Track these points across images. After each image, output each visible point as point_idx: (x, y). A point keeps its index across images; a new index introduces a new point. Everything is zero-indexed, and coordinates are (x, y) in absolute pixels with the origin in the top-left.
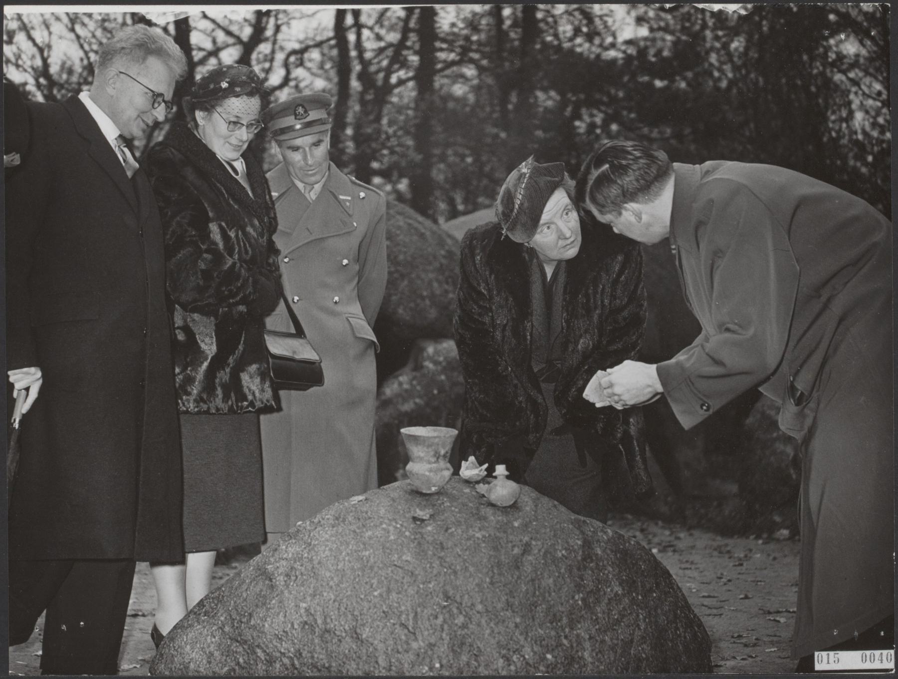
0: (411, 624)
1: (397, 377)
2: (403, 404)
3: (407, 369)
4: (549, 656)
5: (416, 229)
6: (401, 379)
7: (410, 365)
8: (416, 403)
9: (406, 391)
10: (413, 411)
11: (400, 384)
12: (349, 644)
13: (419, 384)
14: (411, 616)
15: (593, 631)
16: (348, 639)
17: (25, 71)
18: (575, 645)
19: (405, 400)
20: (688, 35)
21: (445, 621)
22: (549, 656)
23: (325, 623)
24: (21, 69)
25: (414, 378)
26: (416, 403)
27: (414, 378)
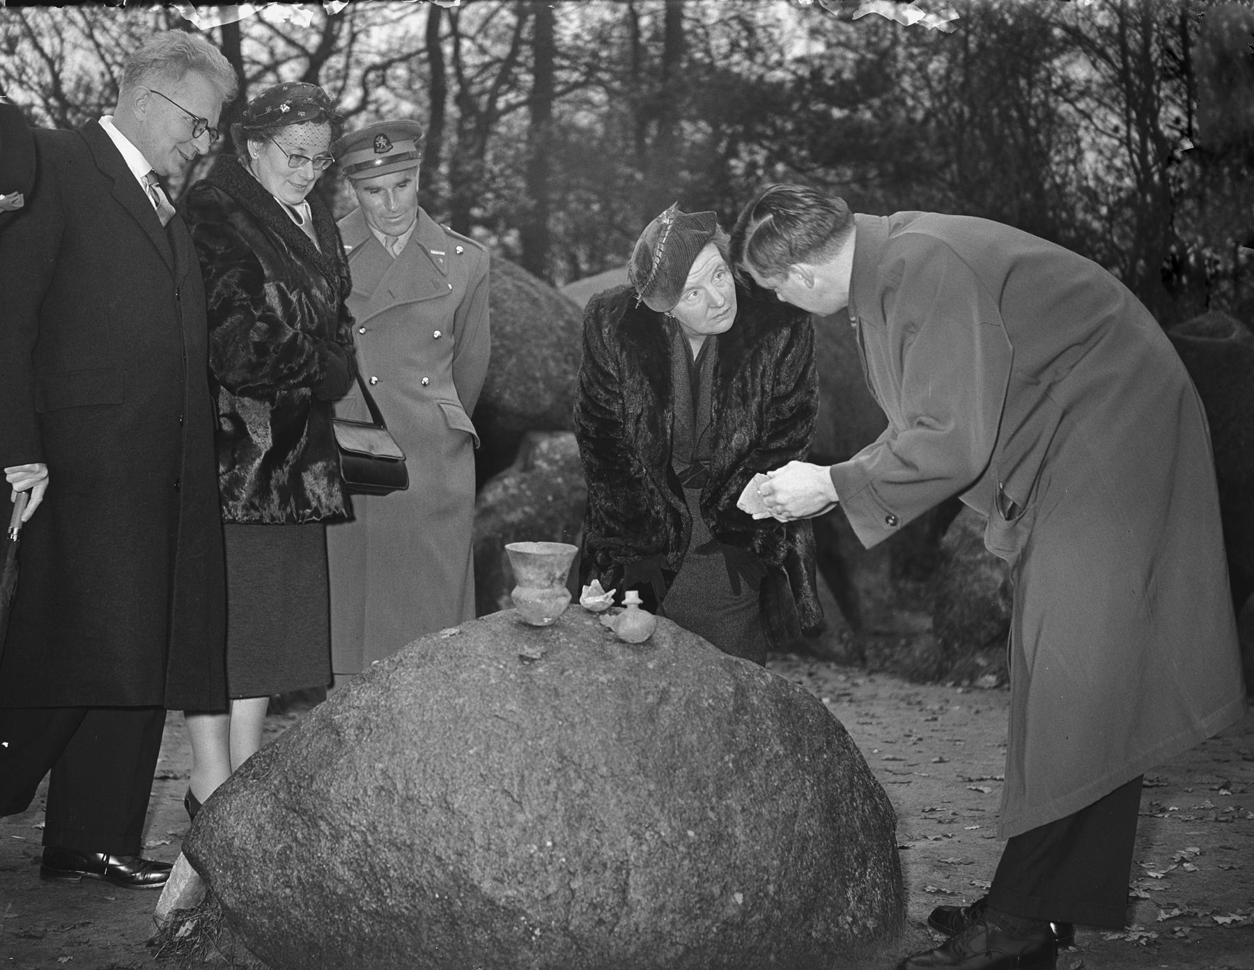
2: (508, 513)
4: (691, 833)
5: (527, 294)
6: (506, 481)
7: (519, 464)
8: (525, 513)
9: (513, 496)
10: (521, 522)
11: (506, 488)
12: (436, 816)
13: (529, 488)
14: (516, 780)
15: (747, 801)
23: (406, 788)
25: (523, 481)
27: (523, 481)
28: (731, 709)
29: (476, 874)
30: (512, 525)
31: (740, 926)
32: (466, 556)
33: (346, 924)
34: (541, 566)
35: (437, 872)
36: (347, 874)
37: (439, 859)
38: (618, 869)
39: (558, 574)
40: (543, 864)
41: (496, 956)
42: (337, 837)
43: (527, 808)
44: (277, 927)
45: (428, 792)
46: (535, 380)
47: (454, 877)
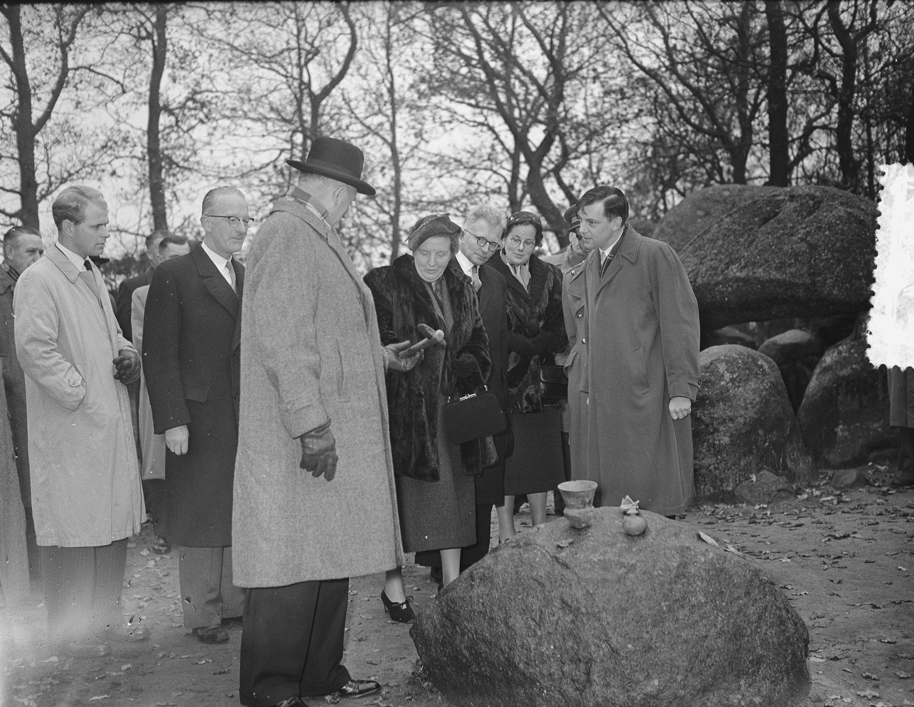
0: (538, 619)
1: (838, 346)
2: (841, 370)
3: (848, 340)
4: (630, 646)
5: (856, 217)
6: (840, 348)
7: (852, 336)
8: (852, 368)
9: (845, 358)
10: (850, 375)
11: (840, 353)
12: (502, 627)
13: (856, 352)
14: (538, 613)
15: (673, 628)
16: (502, 625)
17: (111, 231)
18: (654, 638)
19: (843, 366)
20: (832, 106)
21: (559, 618)
22: (630, 646)
23: (491, 613)
24: (115, 229)
25: (853, 347)
26: (852, 368)
27: (853, 347)
28: (672, 576)
29: (517, 660)
30: (844, 378)
31: (655, 697)
32: (393, 544)
33: (467, 677)
34: (578, 498)
35: (501, 657)
36: (466, 653)
37: (501, 650)
38: (587, 663)
39: (587, 501)
40: (548, 657)
41: (527, 701)
42: (463, 634)
43: (542, 629)
44: (442, 675)
45: (499, 615)
46: (859, 278)
47: (508, 660)
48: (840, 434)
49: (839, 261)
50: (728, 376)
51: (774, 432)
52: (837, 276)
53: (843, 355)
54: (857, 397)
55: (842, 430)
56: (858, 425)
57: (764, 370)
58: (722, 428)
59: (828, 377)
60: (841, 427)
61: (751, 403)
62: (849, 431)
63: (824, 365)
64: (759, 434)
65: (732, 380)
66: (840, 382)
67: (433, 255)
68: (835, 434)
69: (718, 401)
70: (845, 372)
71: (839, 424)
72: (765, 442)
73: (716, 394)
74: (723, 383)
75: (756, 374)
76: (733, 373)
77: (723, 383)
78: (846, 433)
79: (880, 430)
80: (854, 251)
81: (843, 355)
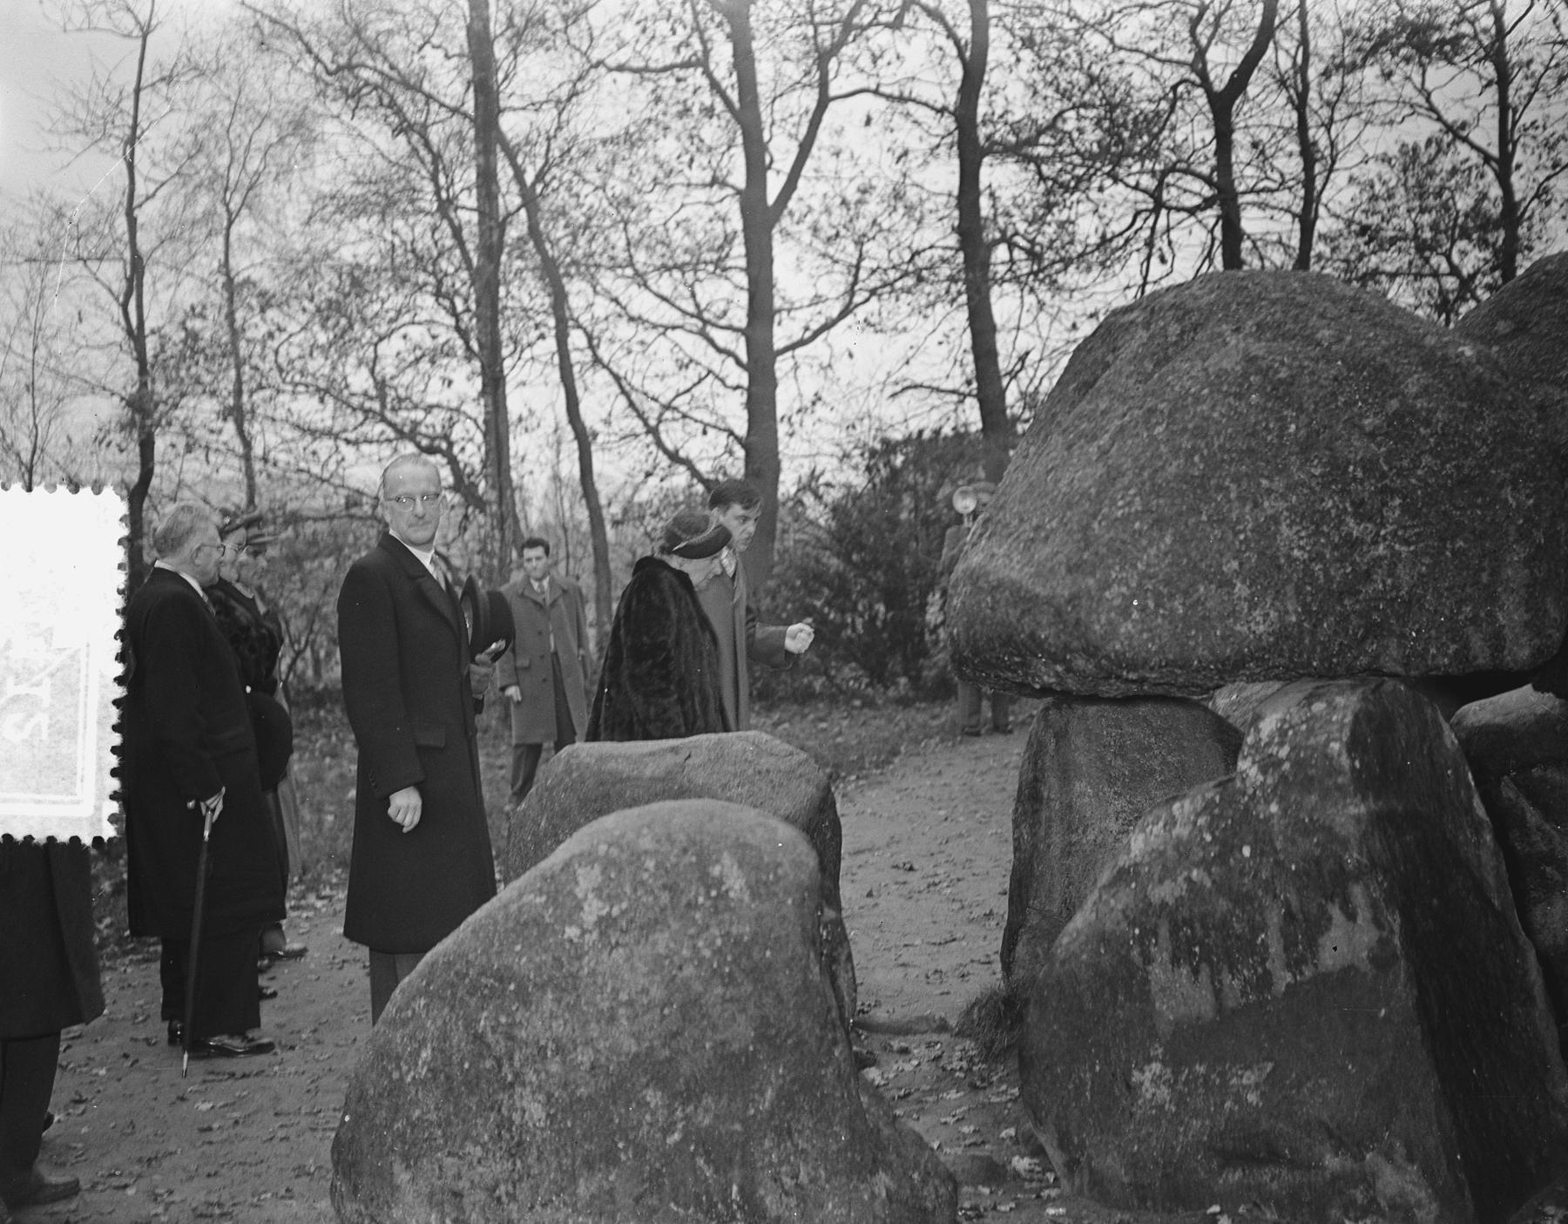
11: (1171, 822)
19: (1167, 873)
26: (1189, 880)
48: (1148, 1090)
49: (1159, 523)
50: (593, 910)
51: (708, 1100)
52: (1144, 576)
53: (1177, 831)
54: (1204, 975)
55: (1156, 1080)
56: (1200, 1069)
57: (723, 896)
58: (531, 1077)
59: (1123, 899)
60: (1156, 1067)
61: (630, 1003)
62: (1171, 1086)
63: (1123, 861)
64: (643, 1104)
65: (605, 923)
66: (1145, 917)
67: (418, 500)
68: (1132, 1089)
69: (542, 987)
70: (1165, 892)
71: (1149, 1060)
72: (667, 1130)
73: (539, 968)
74: (572, 932)
75: (692, 906)
76: (612, 899)
77: (572, 932)
78: (1164, 1093)
79: (1252, 1098)
80: (1220, 488)
81: (1177, 831)
